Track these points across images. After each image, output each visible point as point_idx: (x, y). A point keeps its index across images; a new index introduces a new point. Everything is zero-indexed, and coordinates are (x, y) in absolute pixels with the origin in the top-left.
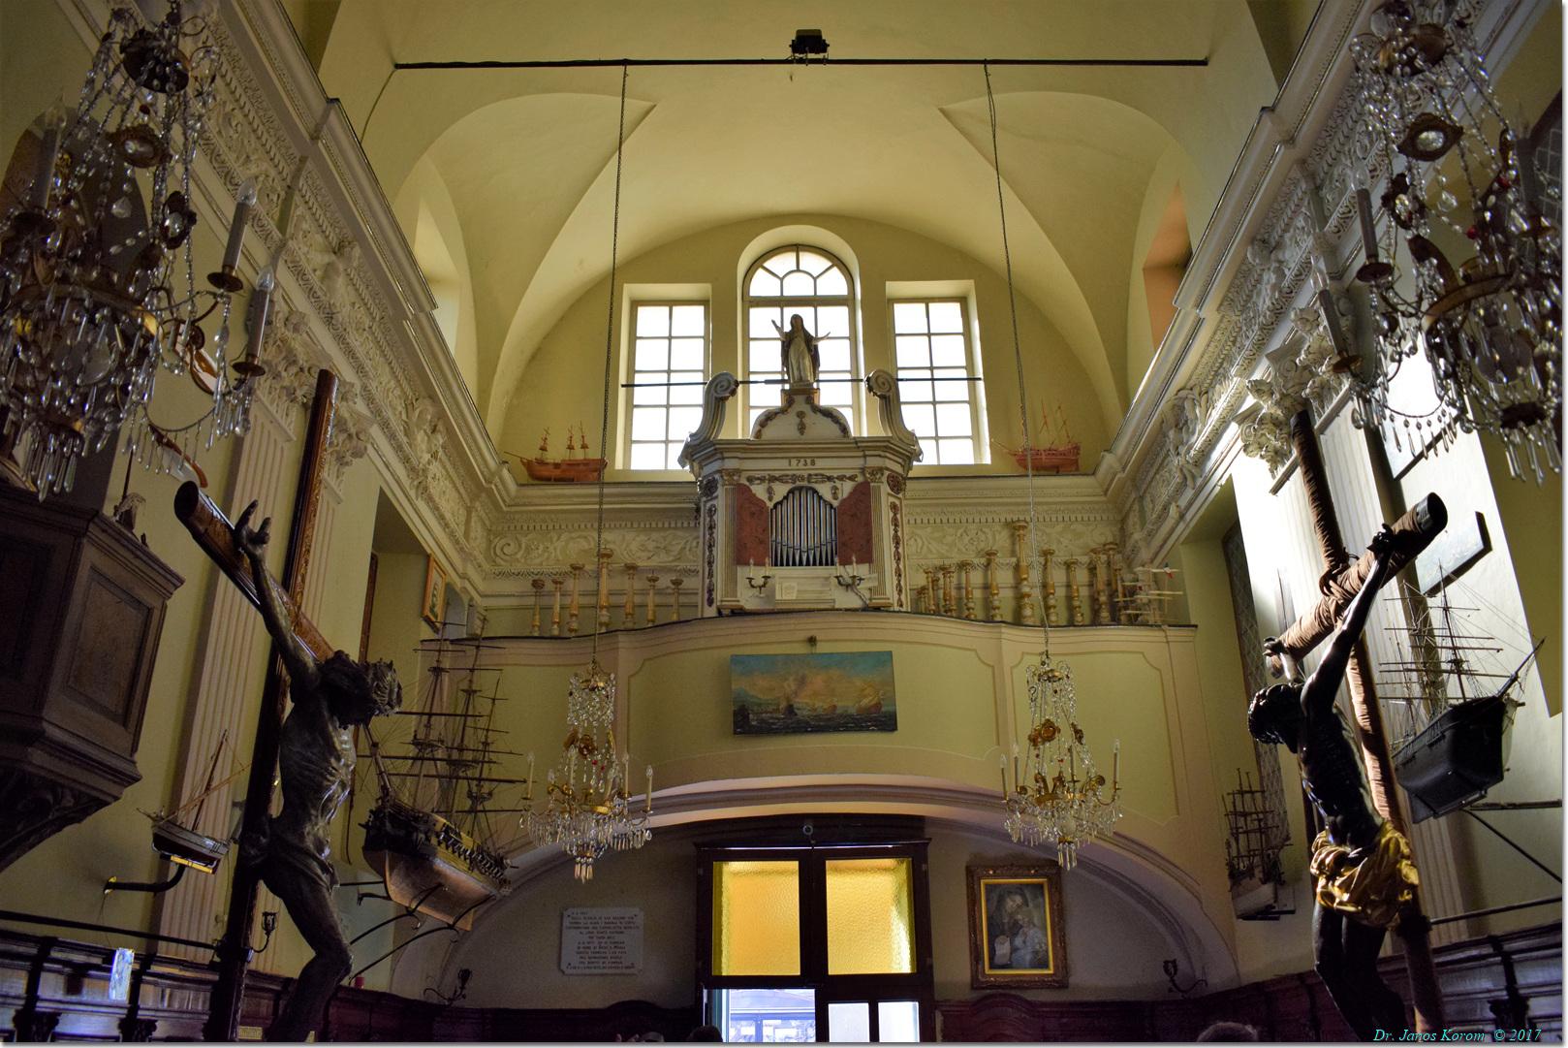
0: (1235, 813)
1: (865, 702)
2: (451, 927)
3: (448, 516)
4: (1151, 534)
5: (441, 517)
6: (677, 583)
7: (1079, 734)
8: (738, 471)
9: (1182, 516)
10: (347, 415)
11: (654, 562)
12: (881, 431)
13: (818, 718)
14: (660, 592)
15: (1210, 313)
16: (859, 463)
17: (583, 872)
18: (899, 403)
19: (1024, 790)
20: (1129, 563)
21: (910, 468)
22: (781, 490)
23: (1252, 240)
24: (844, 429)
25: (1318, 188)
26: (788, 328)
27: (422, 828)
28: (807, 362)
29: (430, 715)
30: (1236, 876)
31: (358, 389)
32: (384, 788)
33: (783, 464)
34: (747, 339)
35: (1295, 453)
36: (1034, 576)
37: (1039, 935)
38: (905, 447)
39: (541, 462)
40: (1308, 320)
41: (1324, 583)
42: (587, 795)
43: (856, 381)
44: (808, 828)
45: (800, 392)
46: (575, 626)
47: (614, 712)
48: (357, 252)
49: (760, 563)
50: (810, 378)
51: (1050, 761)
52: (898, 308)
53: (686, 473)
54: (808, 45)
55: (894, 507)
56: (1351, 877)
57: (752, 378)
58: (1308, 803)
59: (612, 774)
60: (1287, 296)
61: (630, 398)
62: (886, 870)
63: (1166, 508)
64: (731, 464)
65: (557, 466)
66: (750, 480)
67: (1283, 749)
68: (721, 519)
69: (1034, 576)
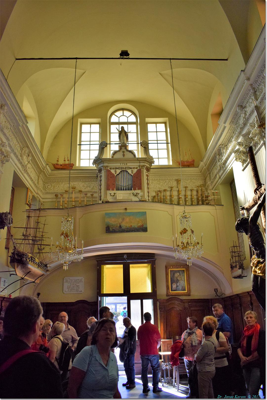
0: (232, 252)
1: (139, 224)
2: (34, 282)
3: (33, 178)
4: (212, 182)
5: (31, 178)
6: (92, 195)
7: (192, 232)
8: (107, 166)
9: (220, 178)
10: (4, 151)
11: (86, 190)
12: (144, 156)
13: (127, 228)
14: (88, 197)
15: (227, 125)
16: (138, 164)
17: (65, 268)
18: (149, 149)
19: (178, 246)
20: (207, 190)
21: (151, 166)
22: (118, 171)
23: (239, 106)
24: (135, 156)
25: (255, 92)
26: (120, 130)
27: (25, 257)
28: (125, 138)
29: (27, 228)
30: (232, 267)
31: (7, 144)
32: (15, 247)
33: (119, 164)
34: (110, 133)
35: (249, 160)
36: (183, 193)
37: (183, 283)
38: (150, 160)
39: (57, 164)
40: (253, 126)
41: (255, 191)
42: (66, 248)
43: (138, 143)
44: (125, 256)
45: (123, 146)
46: (66, 206)
47: (74, 227)
48: (6, 108)
49: (113, 190)
50: (126, 143)
51: (185, 238)
52: (149, 125)
53: (94, 167)
54: (124, 54)
55: (147, 175)
56: (261, 267)
57: (111, 143)
58: (250, 248)
59: (73, 242)
60: (247, 120)
61: (80, 148)
62: (145, 267)
63: (216, 175)
64: (105, 165)
65: (61, 165)
66: (110, 168)
67: (244, 234)
68: (103, 178)
69: (183, 193)
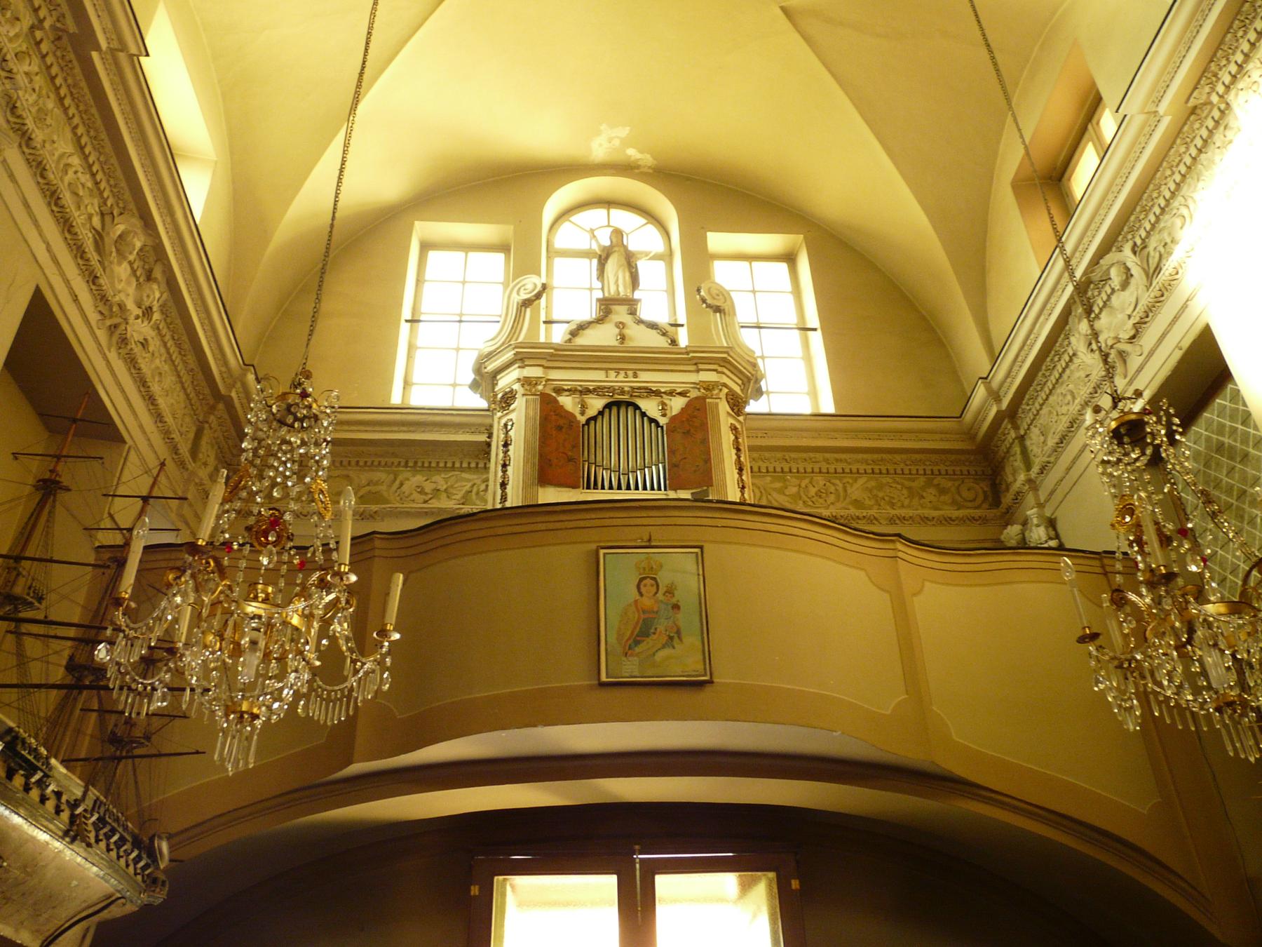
22: (596, 404)
33: (600, 376)
53: (477, 402)
55: (734, 429)
